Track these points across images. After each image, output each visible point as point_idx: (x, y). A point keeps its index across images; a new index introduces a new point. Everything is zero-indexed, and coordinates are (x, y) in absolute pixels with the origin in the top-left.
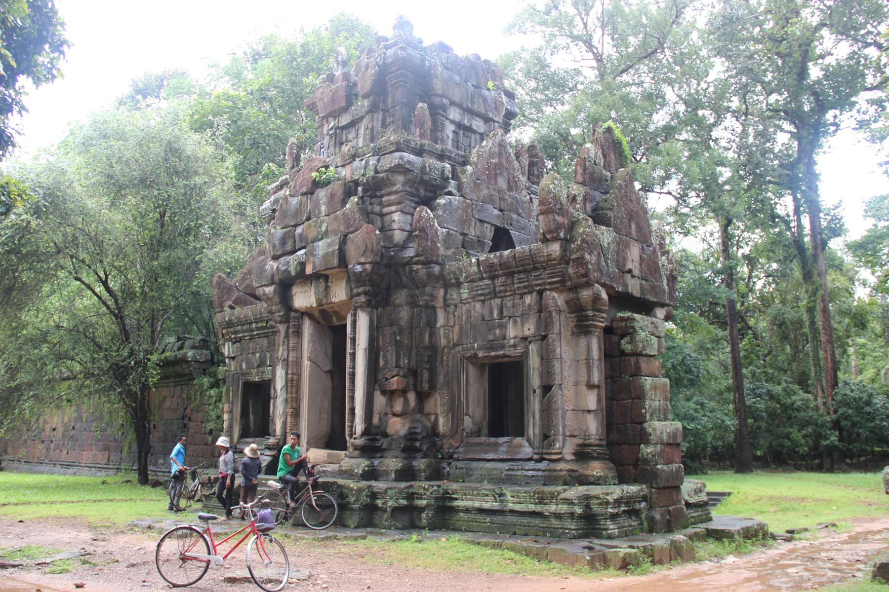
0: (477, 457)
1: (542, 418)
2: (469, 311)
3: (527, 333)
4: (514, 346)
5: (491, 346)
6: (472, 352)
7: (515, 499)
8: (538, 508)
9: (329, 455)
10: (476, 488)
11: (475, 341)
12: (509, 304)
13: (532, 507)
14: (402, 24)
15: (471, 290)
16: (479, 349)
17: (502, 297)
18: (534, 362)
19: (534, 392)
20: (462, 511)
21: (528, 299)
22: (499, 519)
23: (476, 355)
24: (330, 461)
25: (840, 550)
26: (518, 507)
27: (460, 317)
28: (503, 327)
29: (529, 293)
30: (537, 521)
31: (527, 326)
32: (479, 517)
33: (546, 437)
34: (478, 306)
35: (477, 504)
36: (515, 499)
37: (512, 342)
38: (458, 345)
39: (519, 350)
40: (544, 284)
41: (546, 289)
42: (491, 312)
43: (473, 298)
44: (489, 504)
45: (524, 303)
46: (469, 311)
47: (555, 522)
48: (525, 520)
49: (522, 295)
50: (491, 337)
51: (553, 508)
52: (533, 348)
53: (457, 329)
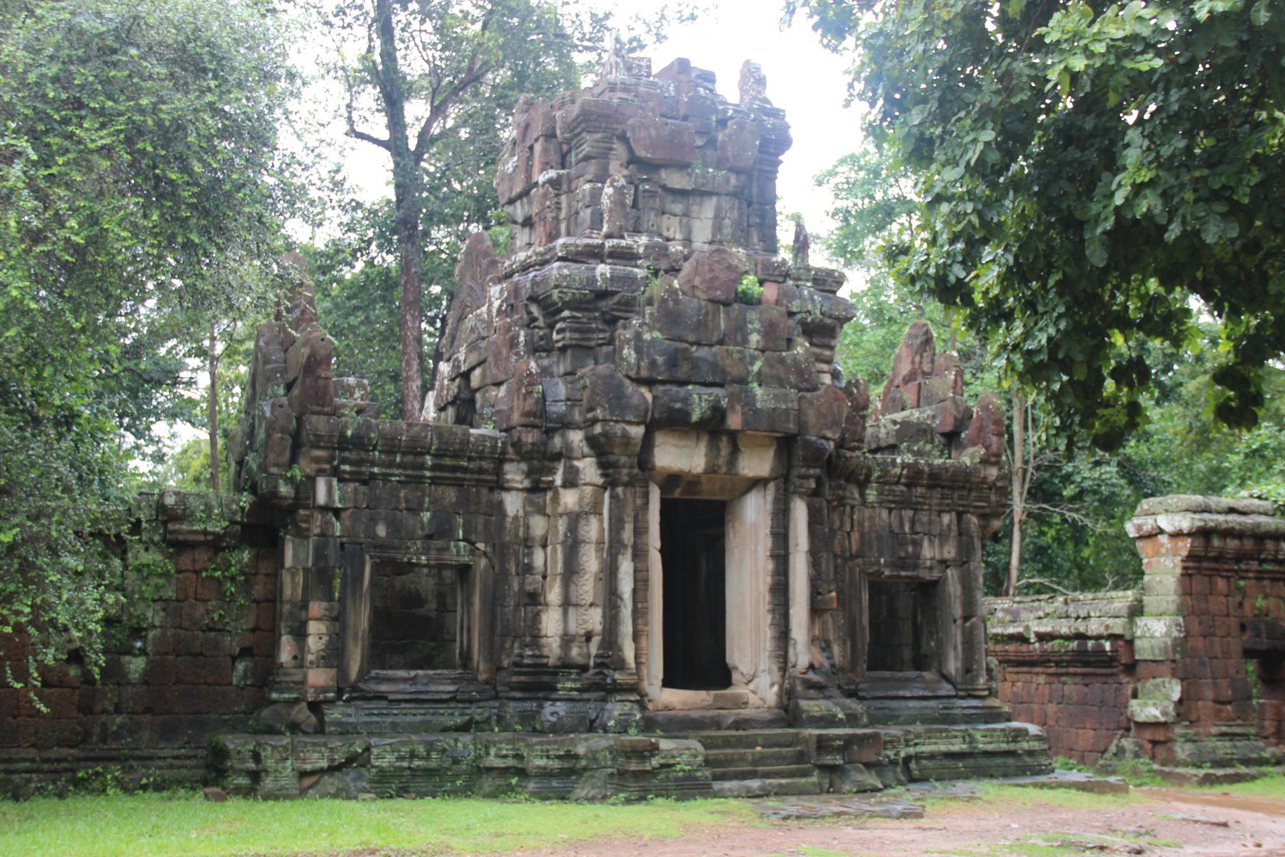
0: (894, 693)
1: (964, 651)
2: (872, 518)
3: (946, 556)
4: (931, 568)
5: (901, 563)
6: (876, 568)
7: (988, 739)
8: (1012, 747)
9: (716, 698)
10: (946, 731)
11: (881, 555)
12: (925, 519)
13: (1004, 746)
14: (753, 78)
15: (880, 493)
16: (886, 565)
17: (916, 510)
18: (954, 588)
19: (955, 621)
20: (926, 758)
21: (946, 519)
22: (971, 761)
23: (879, 573)
24: (719, 705)
25: (151, 758)
26: (990, 747)
27: (861, 524)
28: (917, 544)
29: (949, 512)
30: (1011, 761)
31: (946, 549)
32: (947, 763)
33: (968, 670)
34: (885, 513)
35: (943, 748)
36: (988, 739)
37: (928, 563)
38: (858, 557)
39: (935, 574)
40: (969, 506)
41: (968, 512)
42: (901, 525)
43: (880, 503)
44: (958, 746)
45: (941, 522)
46: (872, 518)
47: (1028, 760)
48: (999, 761)
49: (940, 513)
50: (902, 554)
51: (1025, 745)
52: (951, 573)
53: (855, 536)
